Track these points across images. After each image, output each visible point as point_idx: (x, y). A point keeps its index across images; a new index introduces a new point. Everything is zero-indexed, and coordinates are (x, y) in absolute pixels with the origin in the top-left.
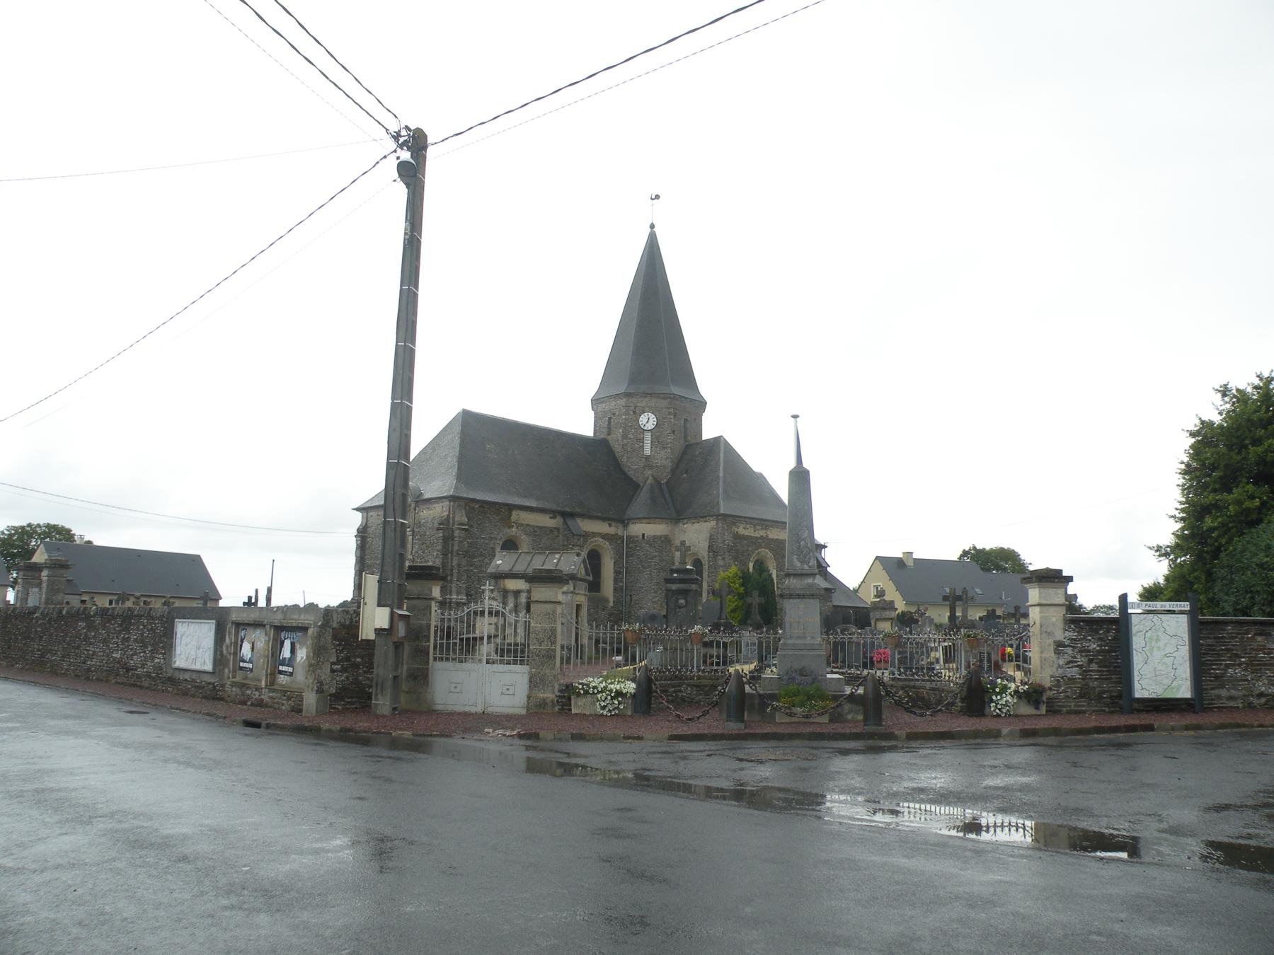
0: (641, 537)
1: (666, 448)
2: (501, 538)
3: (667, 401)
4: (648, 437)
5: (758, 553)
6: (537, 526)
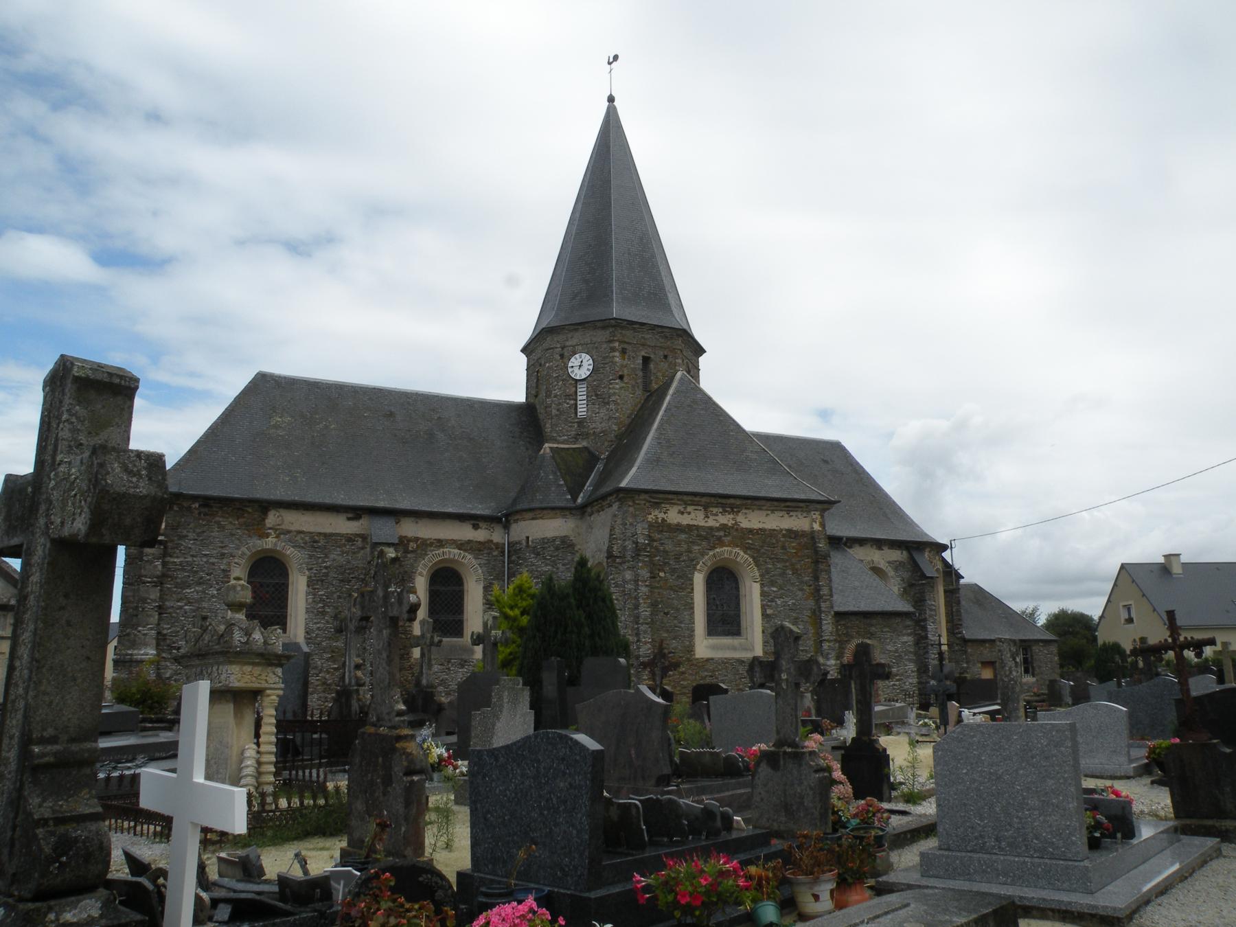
0: (524, 543)
1: (608, 403)
2: (243, 554)
3: (608, 332)
4: (582, 391)
5: (714, 555)
6: (320, 533)
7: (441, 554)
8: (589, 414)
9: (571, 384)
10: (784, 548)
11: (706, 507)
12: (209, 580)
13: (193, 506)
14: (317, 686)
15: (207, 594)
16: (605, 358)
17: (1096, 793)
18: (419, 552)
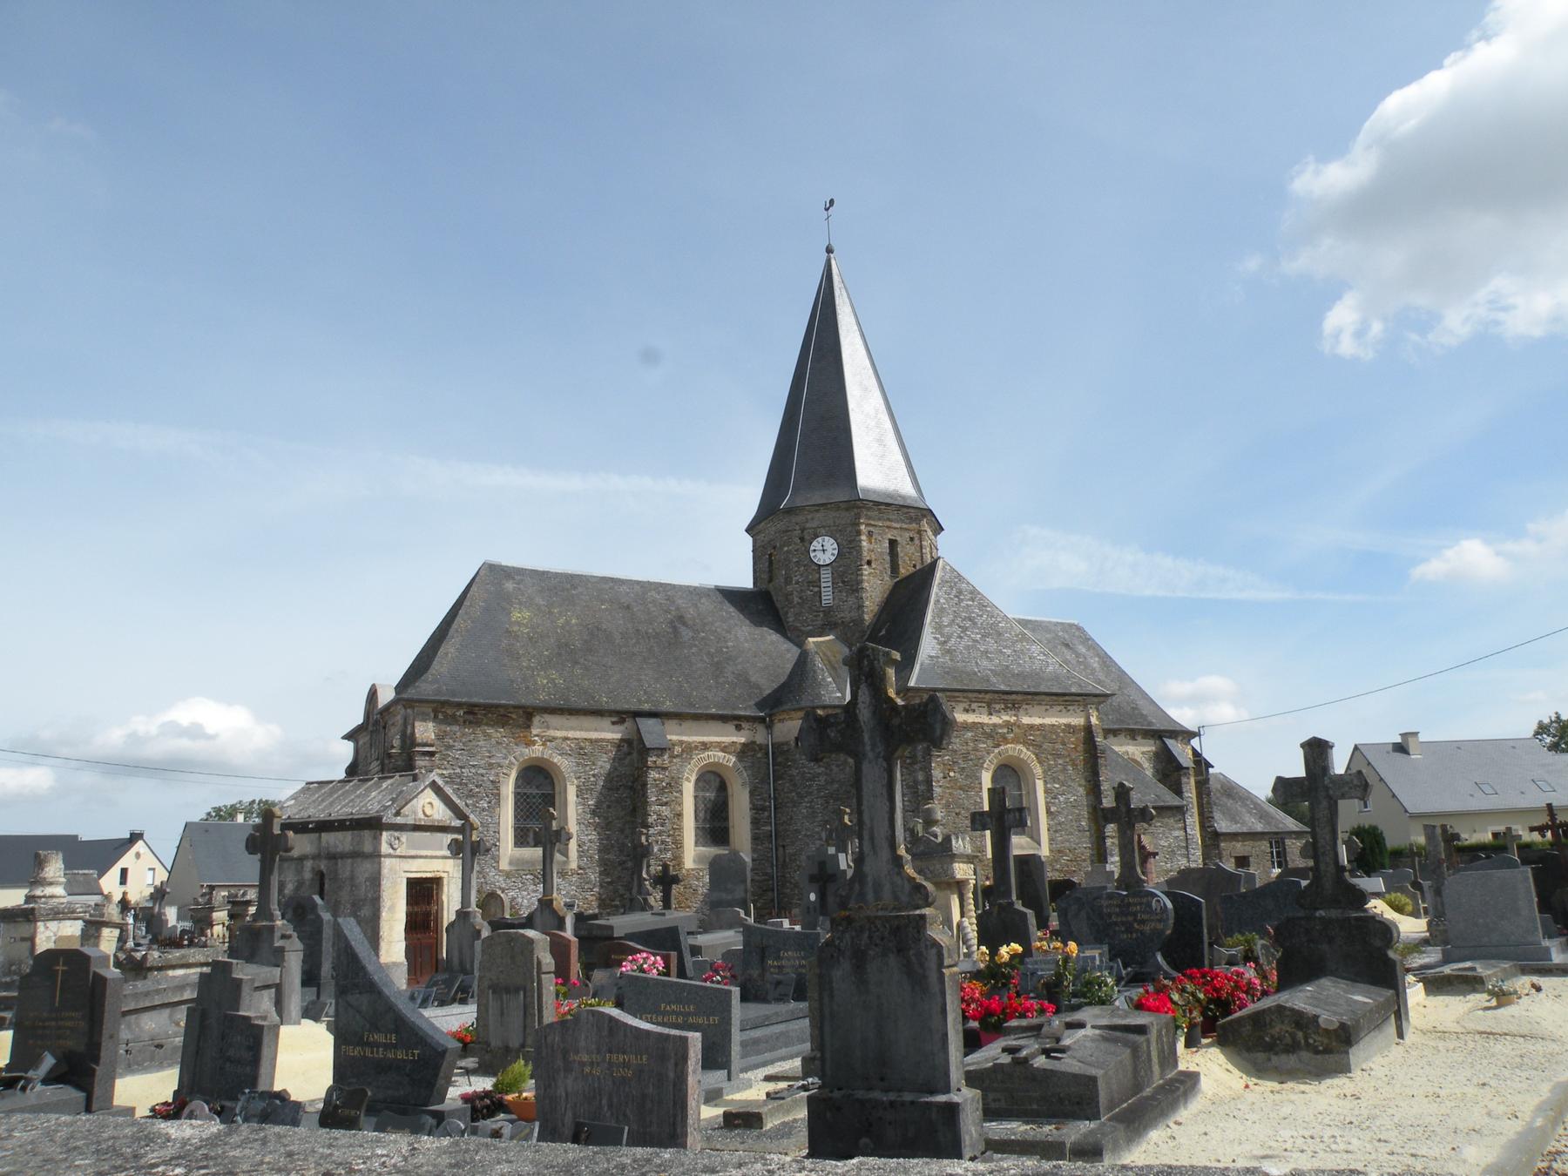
7: (706, 758)
8: (835, 602)
9: (814, 570)
10: (1064, 744)
11: (989, 705)
12: (479, 792)
13: (458, 714)
14: (592, 901)
15: (477, 807)
16: (850, 542)
17: (1163, 1047)
18: (684, 756)
